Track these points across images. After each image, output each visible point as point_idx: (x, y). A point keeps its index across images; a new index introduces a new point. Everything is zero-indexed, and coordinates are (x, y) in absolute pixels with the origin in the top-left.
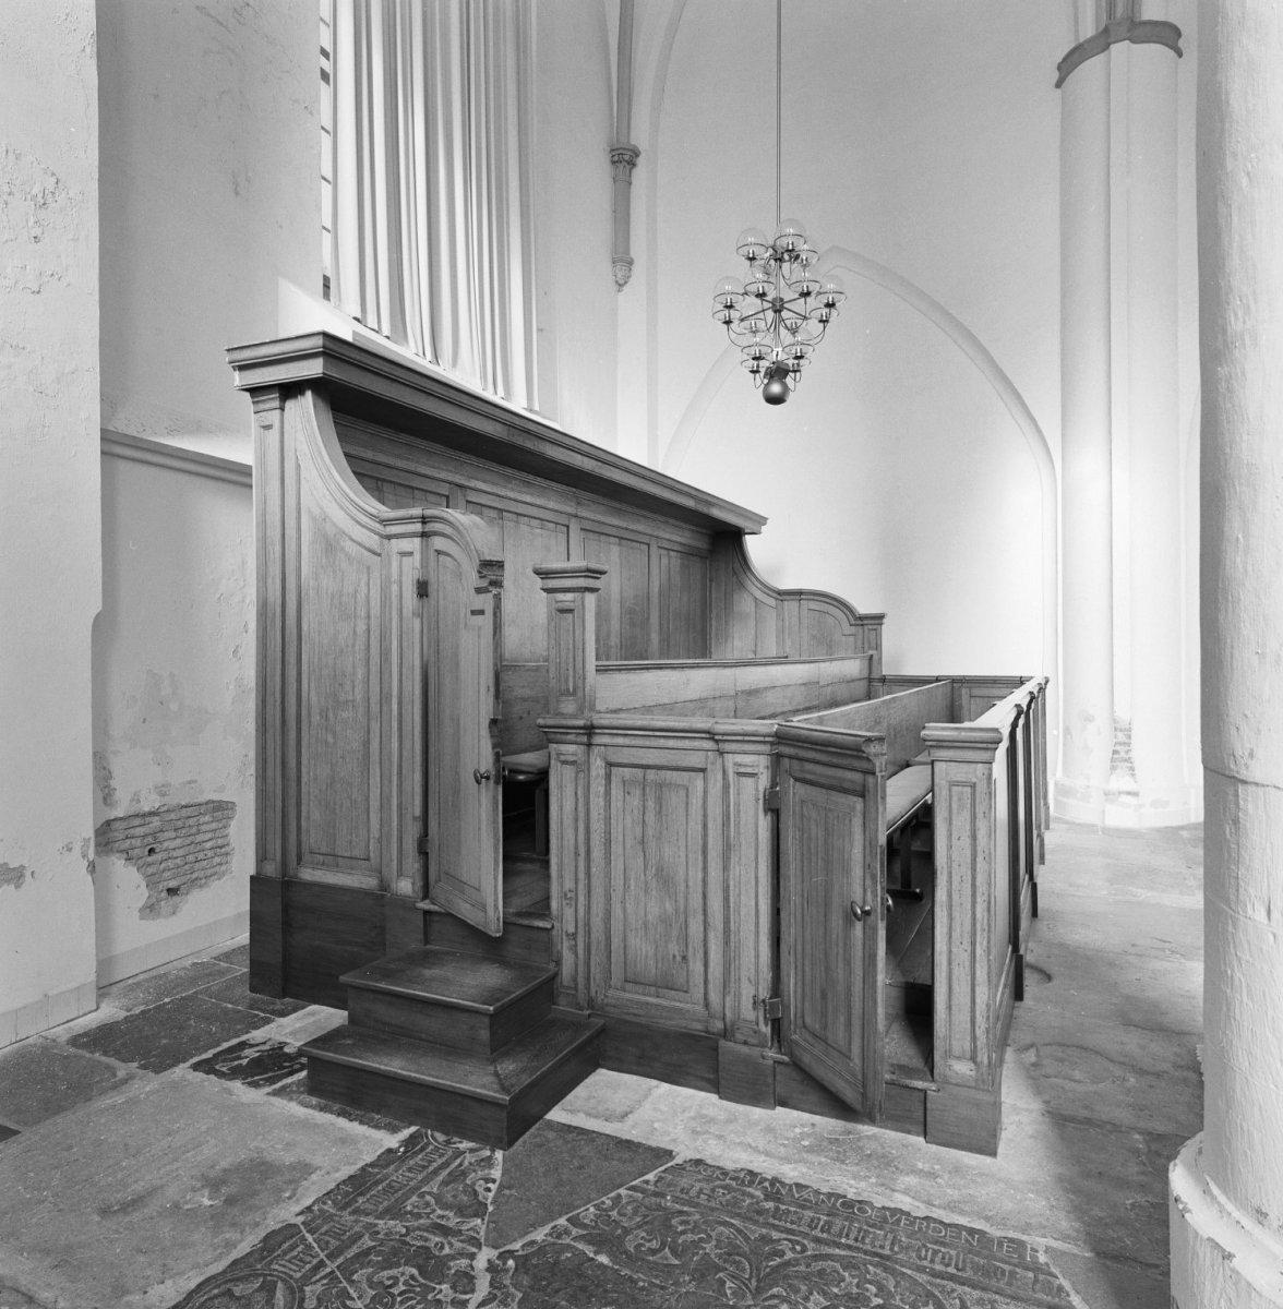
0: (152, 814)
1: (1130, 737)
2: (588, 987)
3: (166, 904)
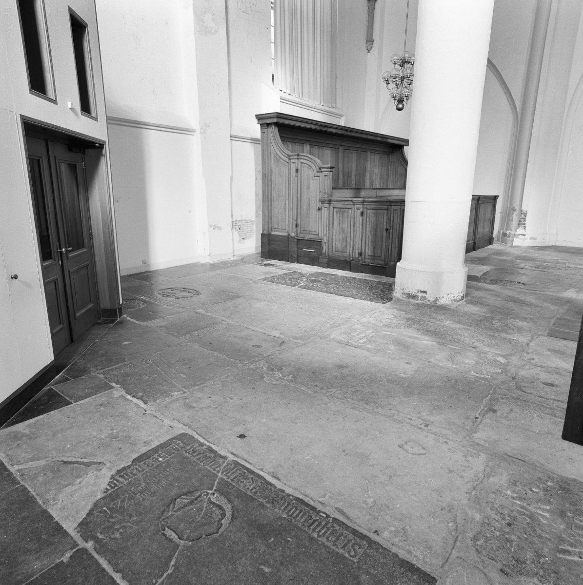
0: (240, 221)
1: (526, 216)
2: (328, 253)
3: (242, 241)
